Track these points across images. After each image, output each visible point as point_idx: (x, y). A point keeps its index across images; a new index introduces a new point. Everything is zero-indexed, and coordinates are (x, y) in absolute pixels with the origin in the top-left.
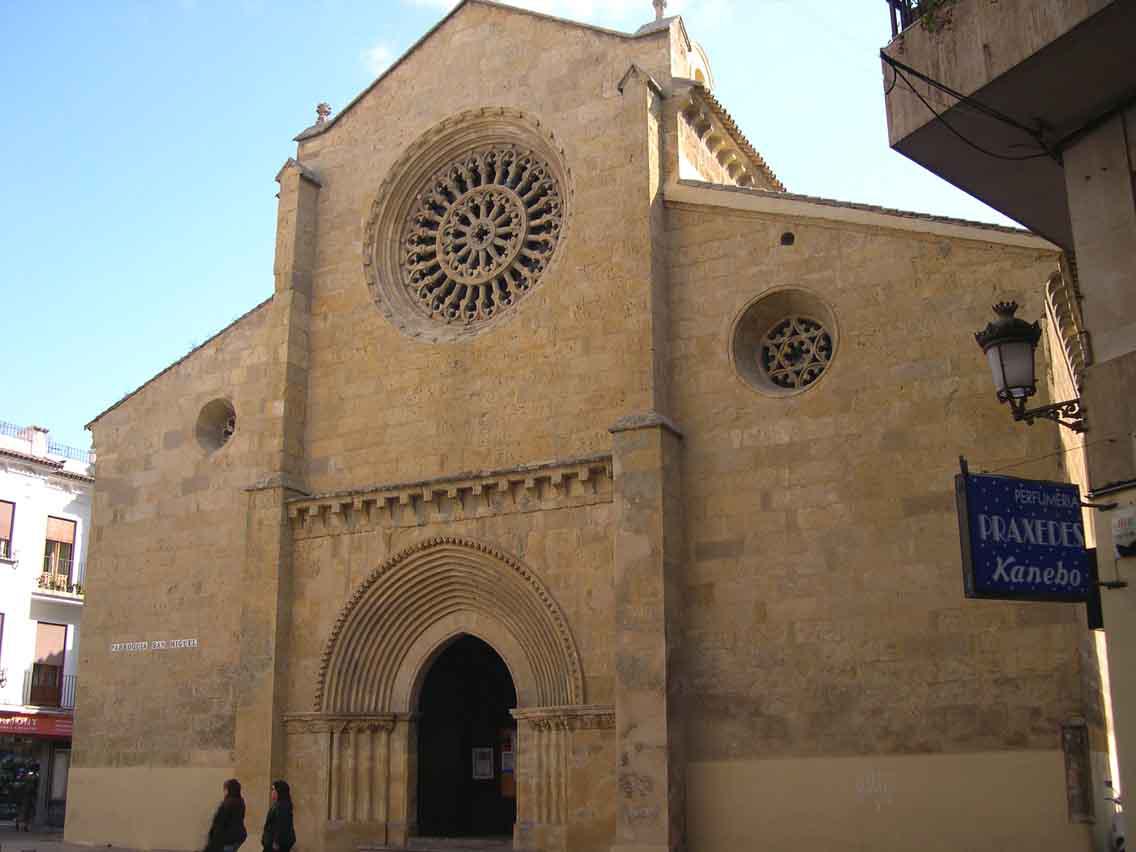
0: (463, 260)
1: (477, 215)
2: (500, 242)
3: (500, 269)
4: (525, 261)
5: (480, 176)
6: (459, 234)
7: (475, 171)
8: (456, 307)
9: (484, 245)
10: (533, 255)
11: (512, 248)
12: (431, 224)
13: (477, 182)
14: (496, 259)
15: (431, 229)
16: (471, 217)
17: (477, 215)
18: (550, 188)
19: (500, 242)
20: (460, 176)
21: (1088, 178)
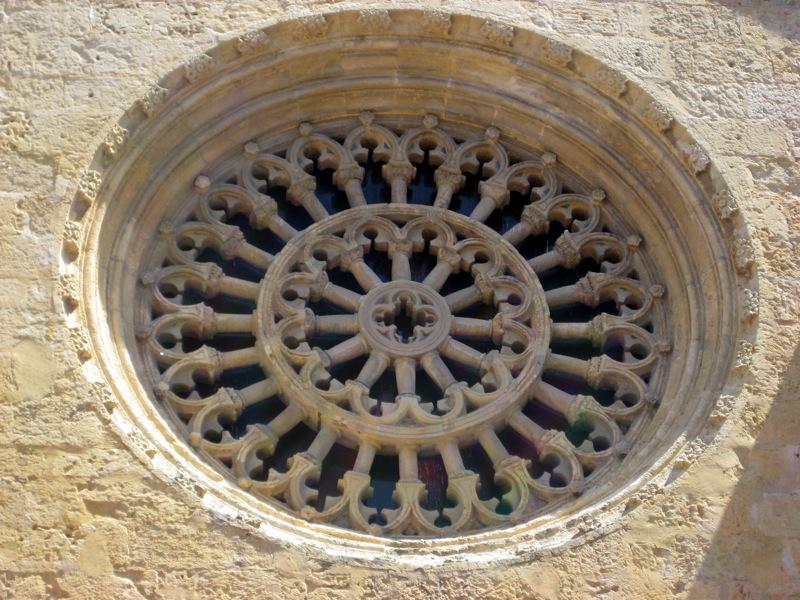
0: (321, 306)
1: (445, 290)
2: (405, 377)
3: (473, 419)
4: (386, 466)
5: (572, 282)
6: (380, 261)
7: (556, 227)
8: (191, 342)
9: (415, 347)
10: (464, 484)
11: (372, 429)
12: (377, 187)
13: (531, 246)
14: (356, 389)
15: (364, 184)
16: (439, 274)
17: (445, 290)
18: (558, 482)
19: (405, 377)
20: (597, 268)
21: (798, 455)
